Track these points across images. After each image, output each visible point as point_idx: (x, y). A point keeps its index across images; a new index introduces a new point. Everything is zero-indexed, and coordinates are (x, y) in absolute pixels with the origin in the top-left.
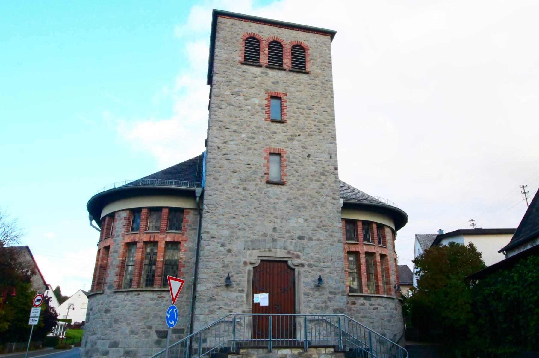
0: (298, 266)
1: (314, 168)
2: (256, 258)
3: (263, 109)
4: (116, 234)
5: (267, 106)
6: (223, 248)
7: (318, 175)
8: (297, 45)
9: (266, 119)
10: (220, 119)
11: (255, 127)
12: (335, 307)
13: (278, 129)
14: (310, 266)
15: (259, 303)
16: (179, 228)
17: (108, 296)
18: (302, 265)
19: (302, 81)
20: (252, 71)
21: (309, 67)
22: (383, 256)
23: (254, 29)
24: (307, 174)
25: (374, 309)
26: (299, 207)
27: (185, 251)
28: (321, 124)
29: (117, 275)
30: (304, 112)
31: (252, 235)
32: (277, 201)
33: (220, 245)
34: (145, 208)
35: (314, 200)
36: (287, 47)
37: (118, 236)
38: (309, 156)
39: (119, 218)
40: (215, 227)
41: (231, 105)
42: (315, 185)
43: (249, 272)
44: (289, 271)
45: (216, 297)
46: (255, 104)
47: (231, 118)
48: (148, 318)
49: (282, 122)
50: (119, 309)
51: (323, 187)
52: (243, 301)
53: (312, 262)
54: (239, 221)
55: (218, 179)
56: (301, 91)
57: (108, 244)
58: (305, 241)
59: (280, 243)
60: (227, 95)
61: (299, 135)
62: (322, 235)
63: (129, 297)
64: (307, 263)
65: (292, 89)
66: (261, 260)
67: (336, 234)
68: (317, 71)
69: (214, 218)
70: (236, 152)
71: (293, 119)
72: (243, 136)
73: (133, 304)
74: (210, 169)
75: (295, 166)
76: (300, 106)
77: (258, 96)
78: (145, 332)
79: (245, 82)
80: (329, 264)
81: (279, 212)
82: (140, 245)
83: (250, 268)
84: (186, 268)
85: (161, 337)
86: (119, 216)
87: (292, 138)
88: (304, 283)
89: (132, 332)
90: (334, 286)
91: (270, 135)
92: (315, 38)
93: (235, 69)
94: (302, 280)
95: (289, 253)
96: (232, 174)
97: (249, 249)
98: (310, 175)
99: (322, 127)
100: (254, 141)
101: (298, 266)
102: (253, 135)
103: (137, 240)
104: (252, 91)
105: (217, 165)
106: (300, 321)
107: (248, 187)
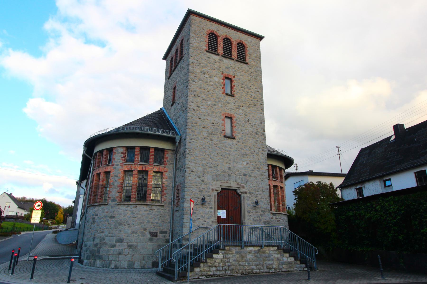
0: (243, 193)
1: (251, 129)
2: (219, 187)
3: (221, 85)
4: (115, 164)
5: (223, 84)
6: (199, 179)
7: (254, 134)
8: (240, 43)
9: (223, 93)
10: (195, 90)
11: (216, 97)
12: (265, 220)
13: (230, 100)
14: (250, 193)
15: (220, 216)
16: (160, 163)
17: (112, 207)
18: (246, 193)
19: (243, 68)
20: (214, 58)
21: (248, 59)
22: (282, 188)
23: (214, 27)
24: (247, 133)
25: (278, 221)
26: (243, 155)
27: (166, 178)
28: (255, 100)
29: (118, 193)
30: (245, 90)
31: (216, 172)
32: (230, 149)
33: (197, 177)
34: (138, 146)
35: (252, 150)
36: (234, 44)
37: (118, 165)
38: (248, 121)
39: (117, 152)
40: (193, 164)
41: (201, 81)
42: (252, 141)
43: (215, 195)
44: (237, 196)
45: (195, 211)
46: (216, 81)
47: (201, 90)
48: (143, 223)
49: (232, 96)
50: (122, 216)
51: (257, 142)
52: (212, 215)
53: (251, 191)
54: (208, 162)
55: (194, 132)
56: (243, 76)
57: (109, 170)
58: (247, 177)
59: (233, 177)
60: (198, 73)
61: (243, 106)
62: (256, 173)
63: (129, 208)
64: (248, 192)
65: (238, 74)
66: (222, 189)
67: (264, 174)
68: (252, 63)
69: (193, 158)
70: (205, 114)
71: (239, 94)
72: (209, 103)
73: (132, 213)
74: (190, 124)
75: (240, 127)
76: (243, 86)
77: (217, 76)
78: (142, 232)
79: (209, 65)
80: (261, 192)
81: (232, 157)
82: (135, 172)
83: (215, 193)
84: (168, 190)
85: (152, 236)
86: (118, 151)
87: (238, 108)
88: (247, 204)
89: (133, 232)
90: (264, 207)
91: (226, 104)
92: (251, 40)
93: (203, 54)
94: (246, 202)
95: (238, 184)
96: (203, 129)
97: (215, 181)
98: (249, 133)
99: (256, 102)
100: (216, 107)
101: (243, 193)
102: (215, 103)
103: (133, 169)
104: (214, 72)
105: (194, 122)
106: (245, 228)
107: (213, 139)
